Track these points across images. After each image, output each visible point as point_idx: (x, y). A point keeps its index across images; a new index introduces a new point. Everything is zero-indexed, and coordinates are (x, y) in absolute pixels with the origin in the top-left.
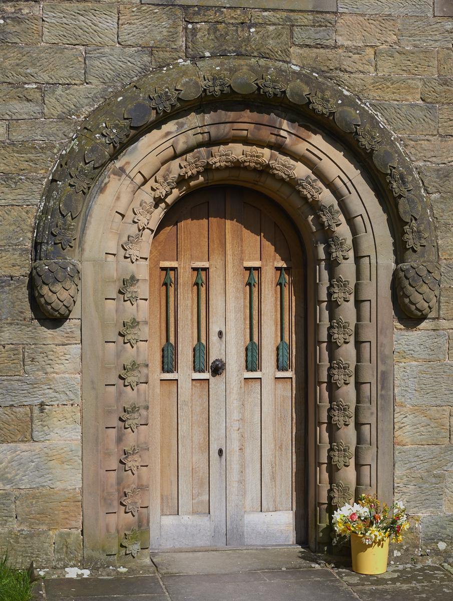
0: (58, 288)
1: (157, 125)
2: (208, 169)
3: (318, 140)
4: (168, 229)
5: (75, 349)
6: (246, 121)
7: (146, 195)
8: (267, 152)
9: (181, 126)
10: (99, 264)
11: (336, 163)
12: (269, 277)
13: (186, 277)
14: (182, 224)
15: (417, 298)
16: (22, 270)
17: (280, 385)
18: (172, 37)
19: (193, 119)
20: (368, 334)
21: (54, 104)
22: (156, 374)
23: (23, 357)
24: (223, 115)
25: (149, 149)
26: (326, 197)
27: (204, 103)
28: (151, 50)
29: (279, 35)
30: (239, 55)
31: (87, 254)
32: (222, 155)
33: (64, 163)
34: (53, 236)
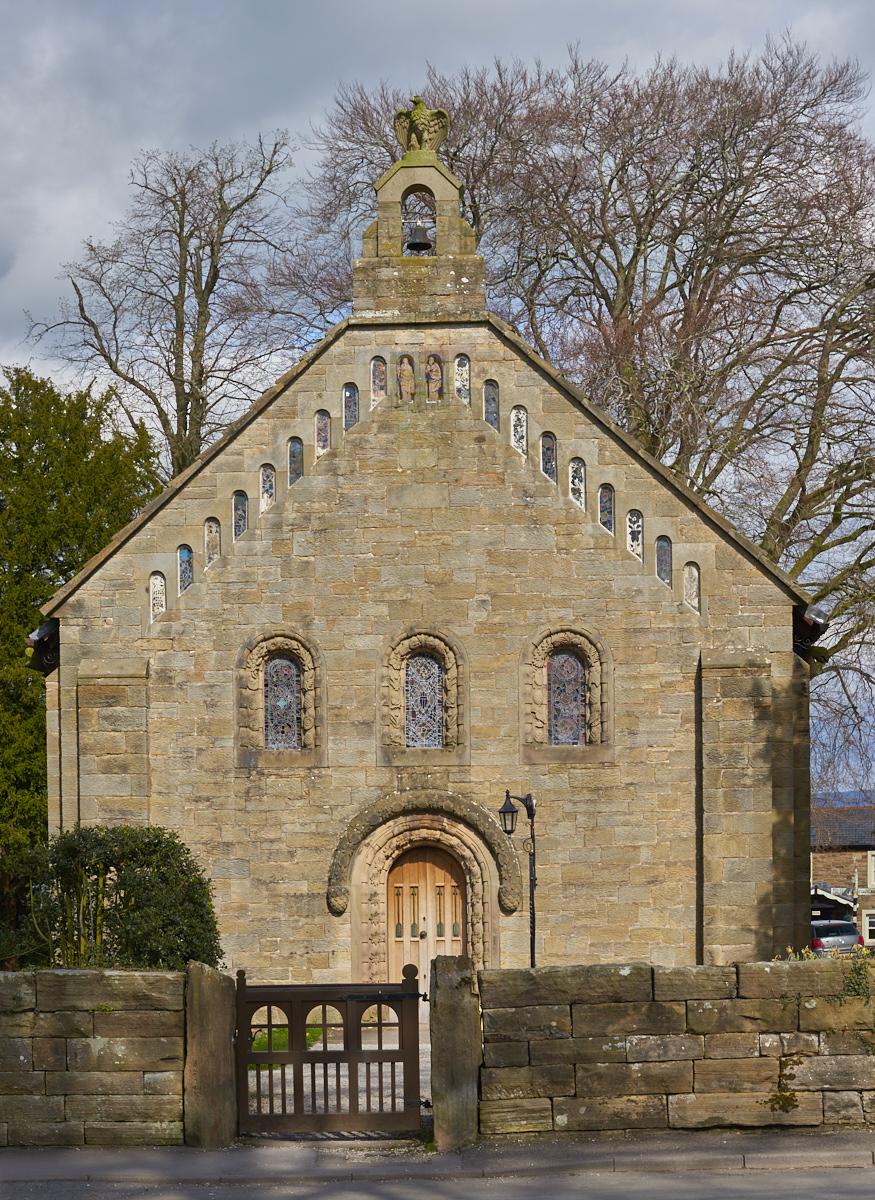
0: (338, 899)
1: (384, 822)
2: (411, 841)
3: (461, 827)
4: (397, 869)
5: (348, 926)
6: (426, 819)
7: (381, 855)
8: (438, 832)
9: (396, 822)
10: (359, 887)
11: (470, 837)
12: (448, 890)
13: (407, 891)
14: (405, 866)
15: (507, 901)
16: (323, 891)
17: (455, 943)
18: (391, 781)
19: (401, 819)
20: (487, 918)
21: (337, 815)
22: (392, 937)
23: (325, 930)
24: (415, 817)
25: (381, 834)
26: (467, 853)
27: (405, 812)
28: (381, 788)
29: (442, 778)
30: (423, 788)
31: (353, 883)
32: (417, 835)
33: (342, 841)
34: (337, 875)
